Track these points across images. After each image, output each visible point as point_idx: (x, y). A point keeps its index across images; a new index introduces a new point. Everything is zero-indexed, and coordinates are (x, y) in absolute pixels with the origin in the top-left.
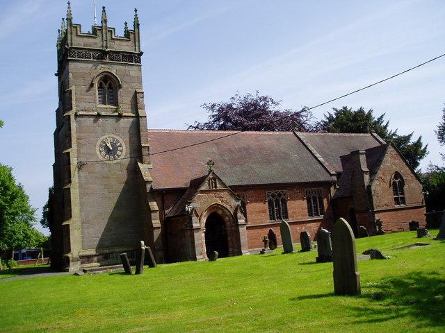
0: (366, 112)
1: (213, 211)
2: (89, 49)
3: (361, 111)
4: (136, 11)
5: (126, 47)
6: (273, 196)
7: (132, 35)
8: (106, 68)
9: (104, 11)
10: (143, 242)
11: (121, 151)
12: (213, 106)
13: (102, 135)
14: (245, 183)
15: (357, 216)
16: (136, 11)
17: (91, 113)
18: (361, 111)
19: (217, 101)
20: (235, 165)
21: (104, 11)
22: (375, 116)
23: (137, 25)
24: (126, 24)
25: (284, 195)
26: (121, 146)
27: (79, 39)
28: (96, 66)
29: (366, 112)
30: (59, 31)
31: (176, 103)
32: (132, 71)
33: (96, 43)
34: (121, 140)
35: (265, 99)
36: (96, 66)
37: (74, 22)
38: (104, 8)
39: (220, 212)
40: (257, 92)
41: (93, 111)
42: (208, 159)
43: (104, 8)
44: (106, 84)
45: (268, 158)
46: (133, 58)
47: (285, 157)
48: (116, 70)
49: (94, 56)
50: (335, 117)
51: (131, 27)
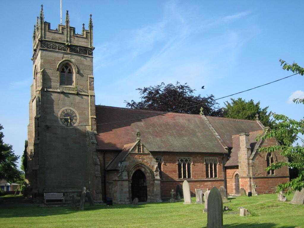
0: (255, 103)
1: (138, 168)
2: (56, 42)
3: (251, 102)
4: (91, 15)
5: (82, 43)
6: (182, 161)
7: (89, 35)
8: (67, 57)
9: (67, 14)
10: (85, 188)
11: (76, 120)
12: (145, 90)
13: (63, 107)
14: (163, 150)
15: (240, 180)
16: (91, 15)
17: (56, 90)
18: (251, 102)
19: (147, 86)
20: (156, 136)
21: (67, 14)
22: (262, 107)
23: (91, 27)
24: (84, 25)
25: (190, 161)
26: (76, 116)
27: (50, 33)
28: (65, 55)
29: (255, 103)
30: (35, 26)
31: (117, 83)
32: (86, 61)
33: (63, 39)
34: (76, 112)
35: (182, 87)
36: (65, 55)
37: (45, 20)
38: (67, 11)
39: (143, 170)
40: (178, 83)
41: (57, 89)
42: (138, 130)
43: (67, 11)
44: (67, 69)
45: (206, 206)
46: (87, 52)
47: (193, 133)
48: (74, 59)
49: (52, 47)
50: (232, 105)
51: (87, 28)
